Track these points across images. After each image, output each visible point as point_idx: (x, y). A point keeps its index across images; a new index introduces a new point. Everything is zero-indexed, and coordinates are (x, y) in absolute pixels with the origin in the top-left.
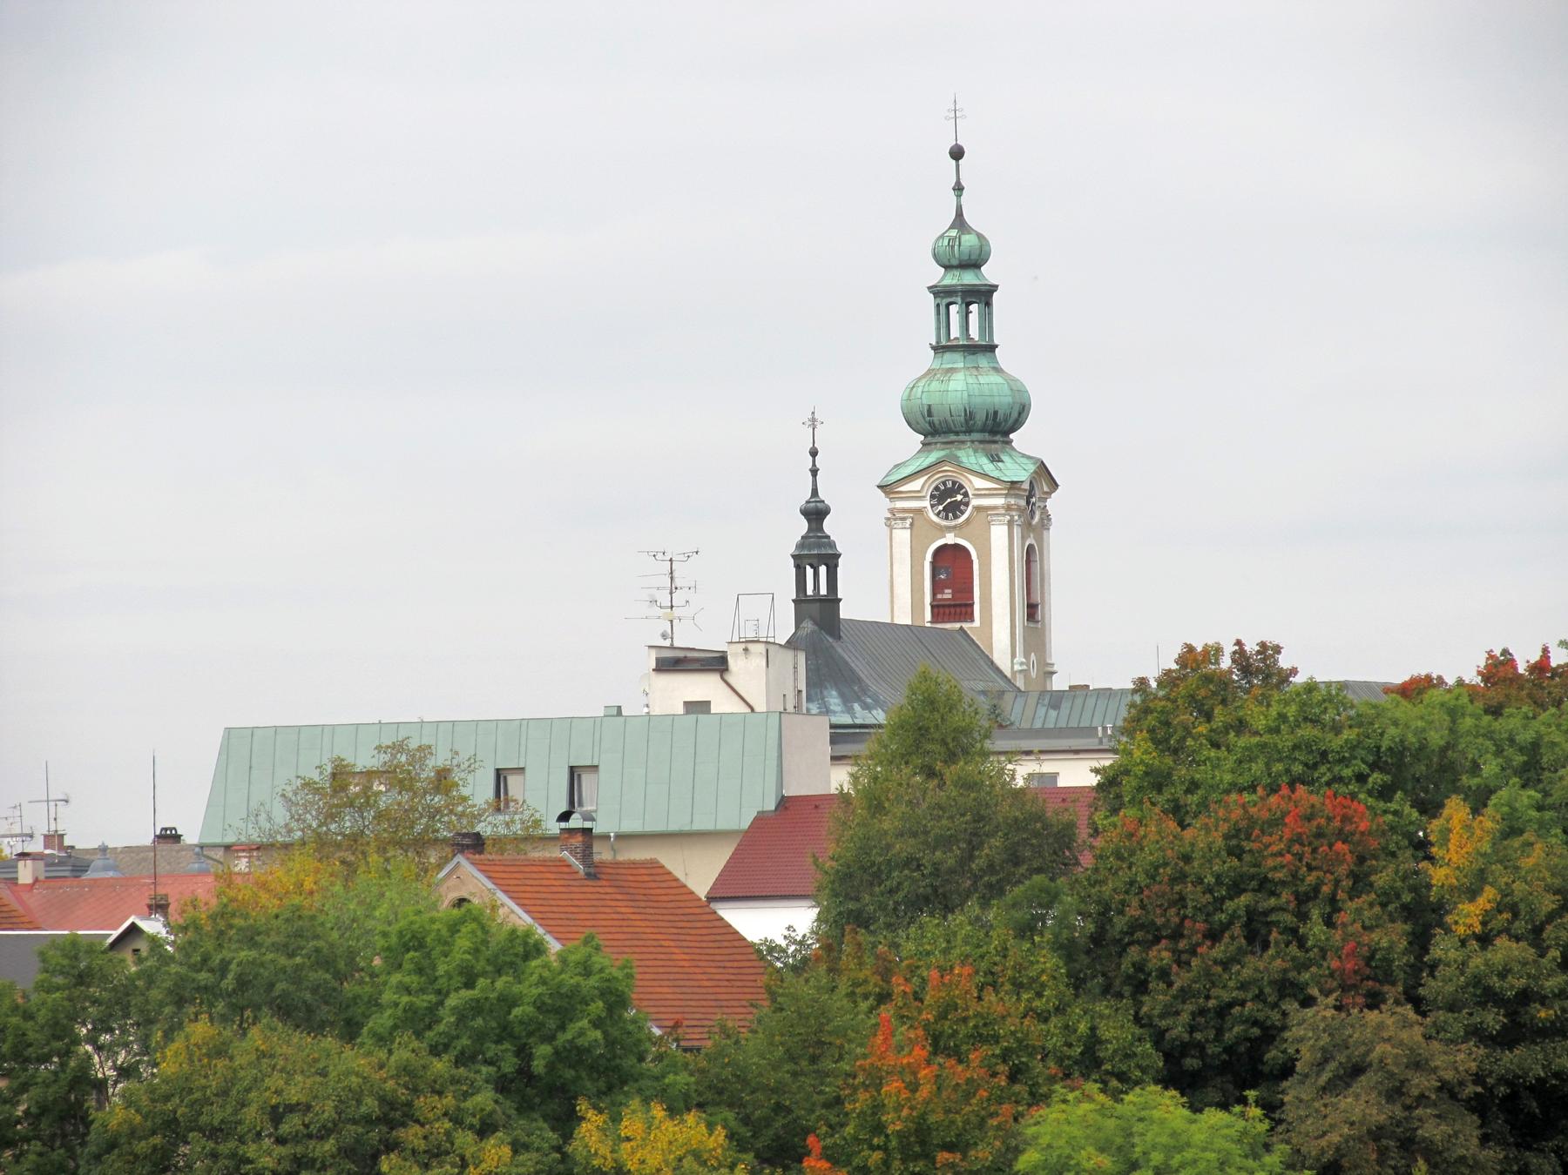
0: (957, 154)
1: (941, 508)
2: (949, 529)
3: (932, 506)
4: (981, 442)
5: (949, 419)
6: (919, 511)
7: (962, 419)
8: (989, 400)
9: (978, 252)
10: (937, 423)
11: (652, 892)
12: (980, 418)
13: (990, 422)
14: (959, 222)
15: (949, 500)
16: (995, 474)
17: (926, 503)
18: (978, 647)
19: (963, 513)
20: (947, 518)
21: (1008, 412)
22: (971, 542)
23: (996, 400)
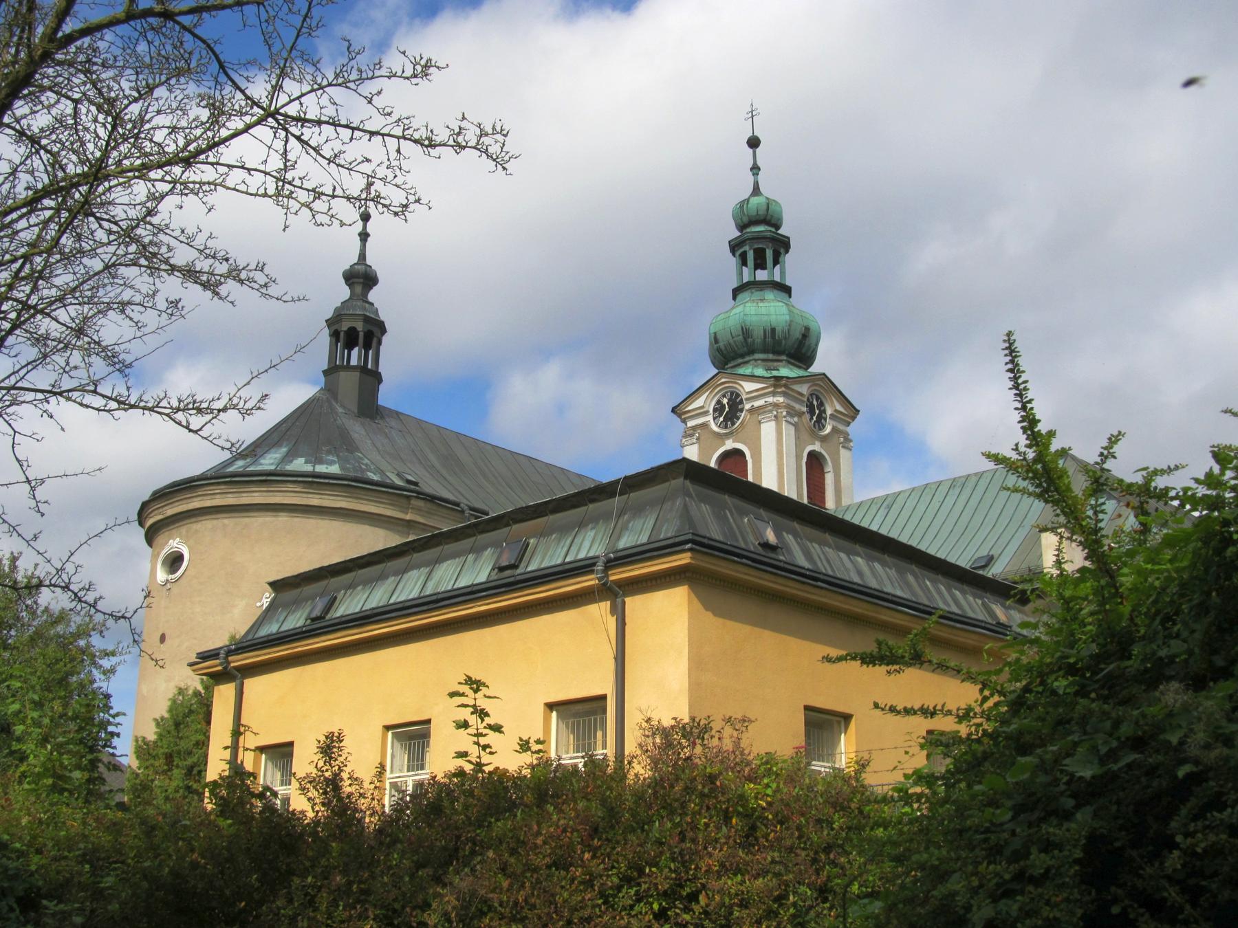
0: (754, 143)
1: (721, 419)
2: (727, 436)
3: (714, 419)
4: (763, 360)
5: (731, 341)
6: (705, 425)
7: (741, 337)
8: (766, 318)
9: (765, 207)
10: (723, 348)
11: (964, 497)
12: (758, 334)
13: (769, 340)
14: (756, 191)
15: (727, 409)
16: (855, 510)
17: (710, 418)
18: (419, 523)
19: (738, 419)
20: (726, 427)
21: (786, 328)
22: (745, 444)
23: (773, 318)
